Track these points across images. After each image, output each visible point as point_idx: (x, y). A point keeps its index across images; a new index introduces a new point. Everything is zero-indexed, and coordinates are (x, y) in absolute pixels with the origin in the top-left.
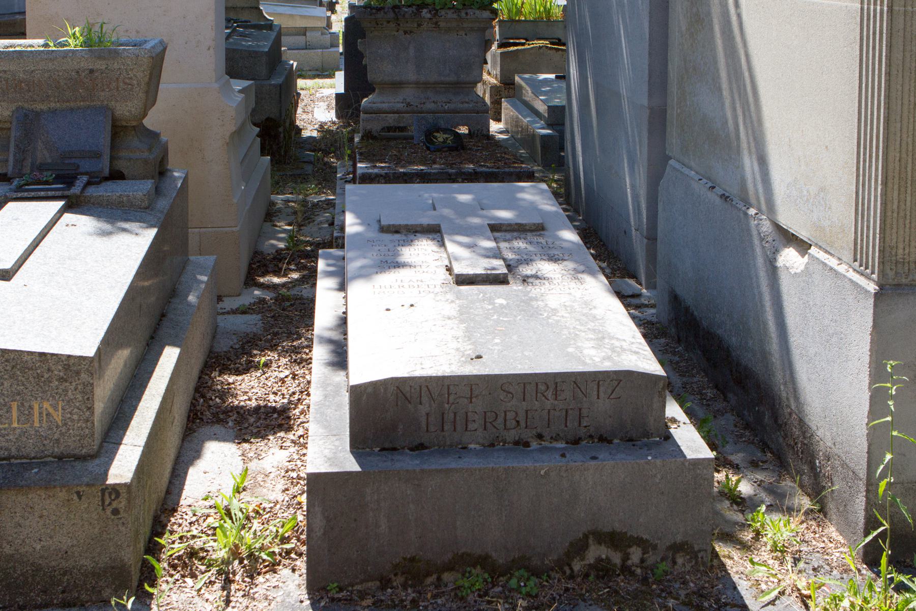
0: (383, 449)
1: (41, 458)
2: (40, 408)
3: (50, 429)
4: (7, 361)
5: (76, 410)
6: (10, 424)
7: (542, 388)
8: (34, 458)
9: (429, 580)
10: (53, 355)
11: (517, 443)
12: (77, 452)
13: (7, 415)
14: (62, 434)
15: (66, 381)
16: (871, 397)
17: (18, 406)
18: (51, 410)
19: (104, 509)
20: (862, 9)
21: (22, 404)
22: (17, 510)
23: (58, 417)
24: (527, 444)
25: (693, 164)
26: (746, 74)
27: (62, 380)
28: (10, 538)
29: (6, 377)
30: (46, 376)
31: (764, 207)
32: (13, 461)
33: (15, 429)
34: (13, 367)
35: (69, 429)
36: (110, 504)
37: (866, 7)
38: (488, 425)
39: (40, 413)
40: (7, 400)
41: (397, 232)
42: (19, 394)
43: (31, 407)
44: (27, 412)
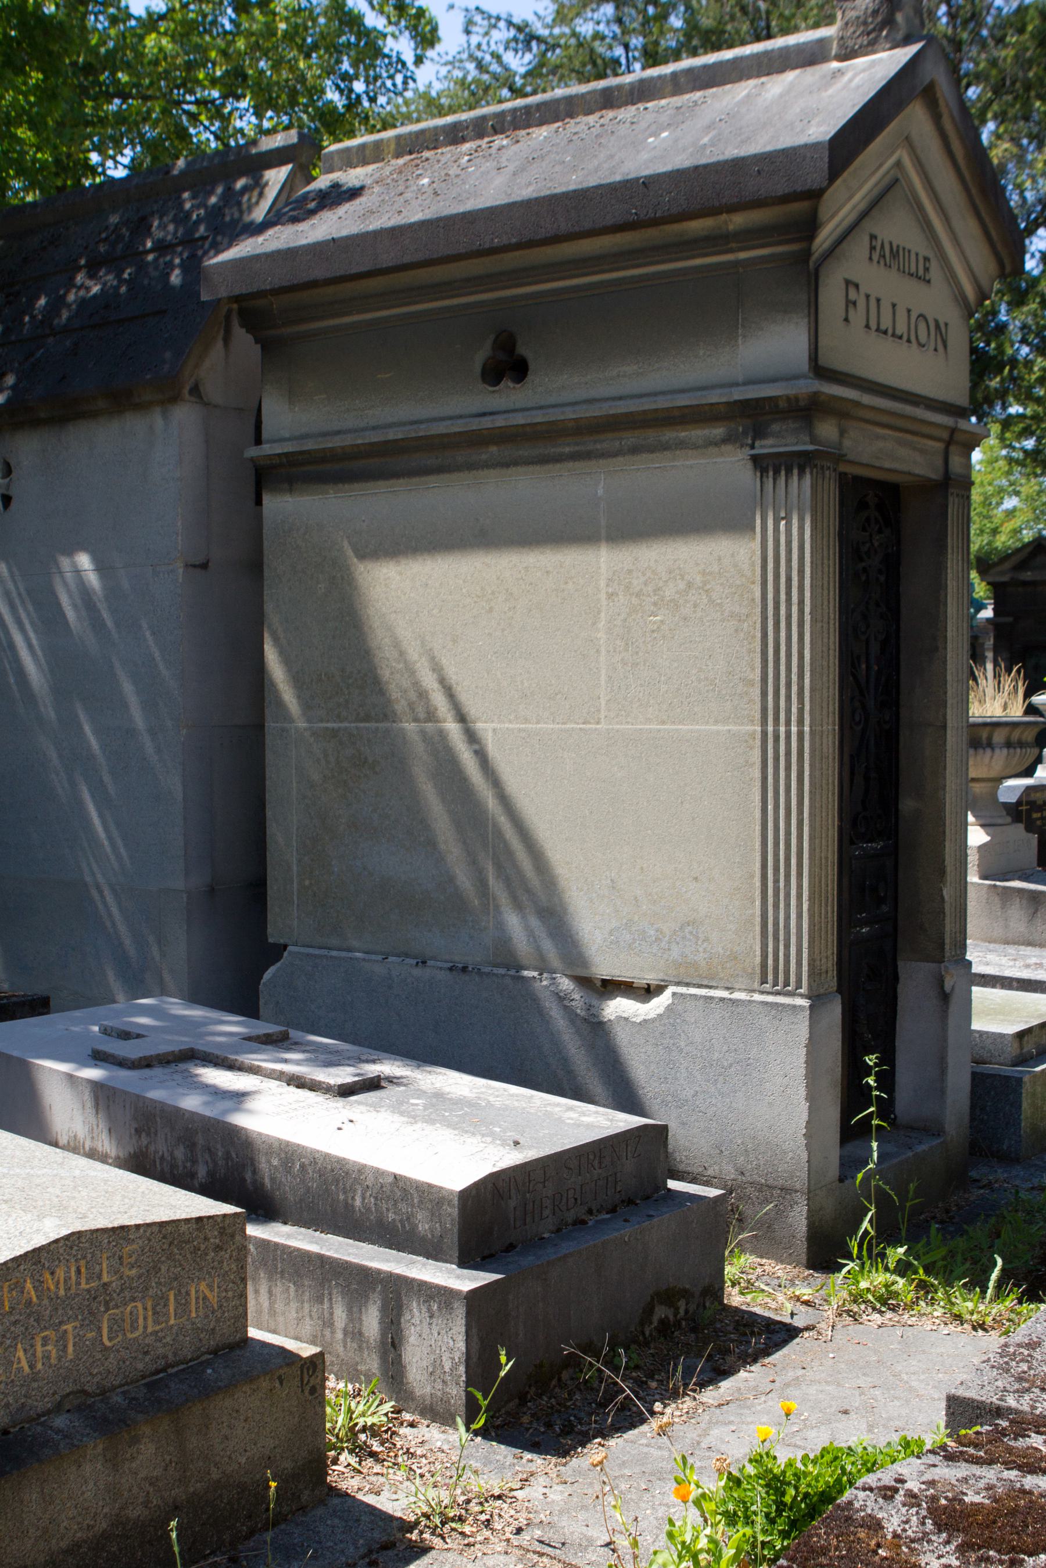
0: (484, 1258)
1: (198, 1358)
2: (197, 1292)
3: (207, 1316)
4: (164, 1237)
5: (231, 1285)
6: (167, 1322)
7: (591, 1157)
8: (190, 1361)
9: (554, 1382)
10: (209, 1217)
11: (574, 1224)
12: (231, 1339)
13: (164, 1310)
14: (218, 1320)
15: (221, 1249)
16: (810, 1107)
17: (175, 1295)
18: (208, 1293)
19: (303, 1391)
20: (764, 733)
21: (179, 1291)
22: (225, 1419)
23: (213, 1297)
24: (583, 1222)
25: (355, 943)
26: (503, 820)
27: (218, 1248)
28: (218, 1458)
29: (163, 1259)
30: (203, 1247)
31: (555, 961)
32: (171, 1371)
33: (172, 1327)
34: (171, 1244)
35: (224, 1312)
36: (309, 1381)
37: (770, 729)
38: (556, 1208)
39: (197, 1298)
40: (164, 1290)
41: (149, 1066)
42: (176, 1279)
43: (188, 1294)
44: (183, 1301)
